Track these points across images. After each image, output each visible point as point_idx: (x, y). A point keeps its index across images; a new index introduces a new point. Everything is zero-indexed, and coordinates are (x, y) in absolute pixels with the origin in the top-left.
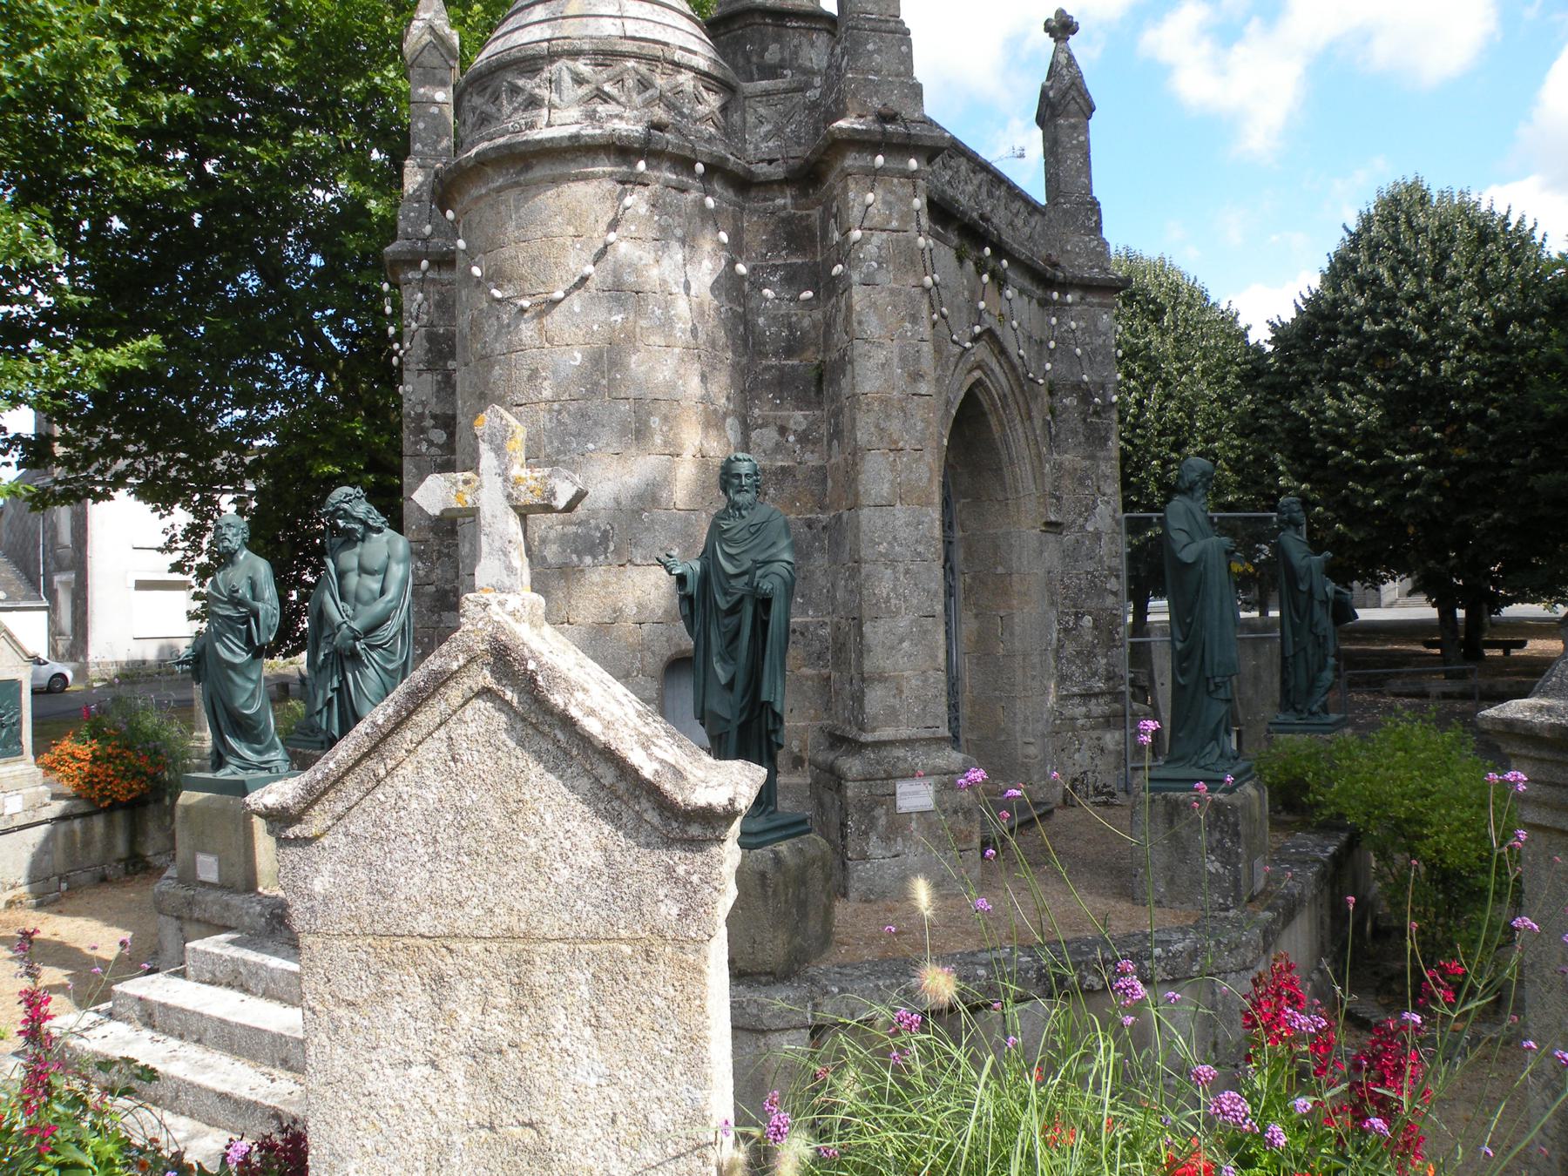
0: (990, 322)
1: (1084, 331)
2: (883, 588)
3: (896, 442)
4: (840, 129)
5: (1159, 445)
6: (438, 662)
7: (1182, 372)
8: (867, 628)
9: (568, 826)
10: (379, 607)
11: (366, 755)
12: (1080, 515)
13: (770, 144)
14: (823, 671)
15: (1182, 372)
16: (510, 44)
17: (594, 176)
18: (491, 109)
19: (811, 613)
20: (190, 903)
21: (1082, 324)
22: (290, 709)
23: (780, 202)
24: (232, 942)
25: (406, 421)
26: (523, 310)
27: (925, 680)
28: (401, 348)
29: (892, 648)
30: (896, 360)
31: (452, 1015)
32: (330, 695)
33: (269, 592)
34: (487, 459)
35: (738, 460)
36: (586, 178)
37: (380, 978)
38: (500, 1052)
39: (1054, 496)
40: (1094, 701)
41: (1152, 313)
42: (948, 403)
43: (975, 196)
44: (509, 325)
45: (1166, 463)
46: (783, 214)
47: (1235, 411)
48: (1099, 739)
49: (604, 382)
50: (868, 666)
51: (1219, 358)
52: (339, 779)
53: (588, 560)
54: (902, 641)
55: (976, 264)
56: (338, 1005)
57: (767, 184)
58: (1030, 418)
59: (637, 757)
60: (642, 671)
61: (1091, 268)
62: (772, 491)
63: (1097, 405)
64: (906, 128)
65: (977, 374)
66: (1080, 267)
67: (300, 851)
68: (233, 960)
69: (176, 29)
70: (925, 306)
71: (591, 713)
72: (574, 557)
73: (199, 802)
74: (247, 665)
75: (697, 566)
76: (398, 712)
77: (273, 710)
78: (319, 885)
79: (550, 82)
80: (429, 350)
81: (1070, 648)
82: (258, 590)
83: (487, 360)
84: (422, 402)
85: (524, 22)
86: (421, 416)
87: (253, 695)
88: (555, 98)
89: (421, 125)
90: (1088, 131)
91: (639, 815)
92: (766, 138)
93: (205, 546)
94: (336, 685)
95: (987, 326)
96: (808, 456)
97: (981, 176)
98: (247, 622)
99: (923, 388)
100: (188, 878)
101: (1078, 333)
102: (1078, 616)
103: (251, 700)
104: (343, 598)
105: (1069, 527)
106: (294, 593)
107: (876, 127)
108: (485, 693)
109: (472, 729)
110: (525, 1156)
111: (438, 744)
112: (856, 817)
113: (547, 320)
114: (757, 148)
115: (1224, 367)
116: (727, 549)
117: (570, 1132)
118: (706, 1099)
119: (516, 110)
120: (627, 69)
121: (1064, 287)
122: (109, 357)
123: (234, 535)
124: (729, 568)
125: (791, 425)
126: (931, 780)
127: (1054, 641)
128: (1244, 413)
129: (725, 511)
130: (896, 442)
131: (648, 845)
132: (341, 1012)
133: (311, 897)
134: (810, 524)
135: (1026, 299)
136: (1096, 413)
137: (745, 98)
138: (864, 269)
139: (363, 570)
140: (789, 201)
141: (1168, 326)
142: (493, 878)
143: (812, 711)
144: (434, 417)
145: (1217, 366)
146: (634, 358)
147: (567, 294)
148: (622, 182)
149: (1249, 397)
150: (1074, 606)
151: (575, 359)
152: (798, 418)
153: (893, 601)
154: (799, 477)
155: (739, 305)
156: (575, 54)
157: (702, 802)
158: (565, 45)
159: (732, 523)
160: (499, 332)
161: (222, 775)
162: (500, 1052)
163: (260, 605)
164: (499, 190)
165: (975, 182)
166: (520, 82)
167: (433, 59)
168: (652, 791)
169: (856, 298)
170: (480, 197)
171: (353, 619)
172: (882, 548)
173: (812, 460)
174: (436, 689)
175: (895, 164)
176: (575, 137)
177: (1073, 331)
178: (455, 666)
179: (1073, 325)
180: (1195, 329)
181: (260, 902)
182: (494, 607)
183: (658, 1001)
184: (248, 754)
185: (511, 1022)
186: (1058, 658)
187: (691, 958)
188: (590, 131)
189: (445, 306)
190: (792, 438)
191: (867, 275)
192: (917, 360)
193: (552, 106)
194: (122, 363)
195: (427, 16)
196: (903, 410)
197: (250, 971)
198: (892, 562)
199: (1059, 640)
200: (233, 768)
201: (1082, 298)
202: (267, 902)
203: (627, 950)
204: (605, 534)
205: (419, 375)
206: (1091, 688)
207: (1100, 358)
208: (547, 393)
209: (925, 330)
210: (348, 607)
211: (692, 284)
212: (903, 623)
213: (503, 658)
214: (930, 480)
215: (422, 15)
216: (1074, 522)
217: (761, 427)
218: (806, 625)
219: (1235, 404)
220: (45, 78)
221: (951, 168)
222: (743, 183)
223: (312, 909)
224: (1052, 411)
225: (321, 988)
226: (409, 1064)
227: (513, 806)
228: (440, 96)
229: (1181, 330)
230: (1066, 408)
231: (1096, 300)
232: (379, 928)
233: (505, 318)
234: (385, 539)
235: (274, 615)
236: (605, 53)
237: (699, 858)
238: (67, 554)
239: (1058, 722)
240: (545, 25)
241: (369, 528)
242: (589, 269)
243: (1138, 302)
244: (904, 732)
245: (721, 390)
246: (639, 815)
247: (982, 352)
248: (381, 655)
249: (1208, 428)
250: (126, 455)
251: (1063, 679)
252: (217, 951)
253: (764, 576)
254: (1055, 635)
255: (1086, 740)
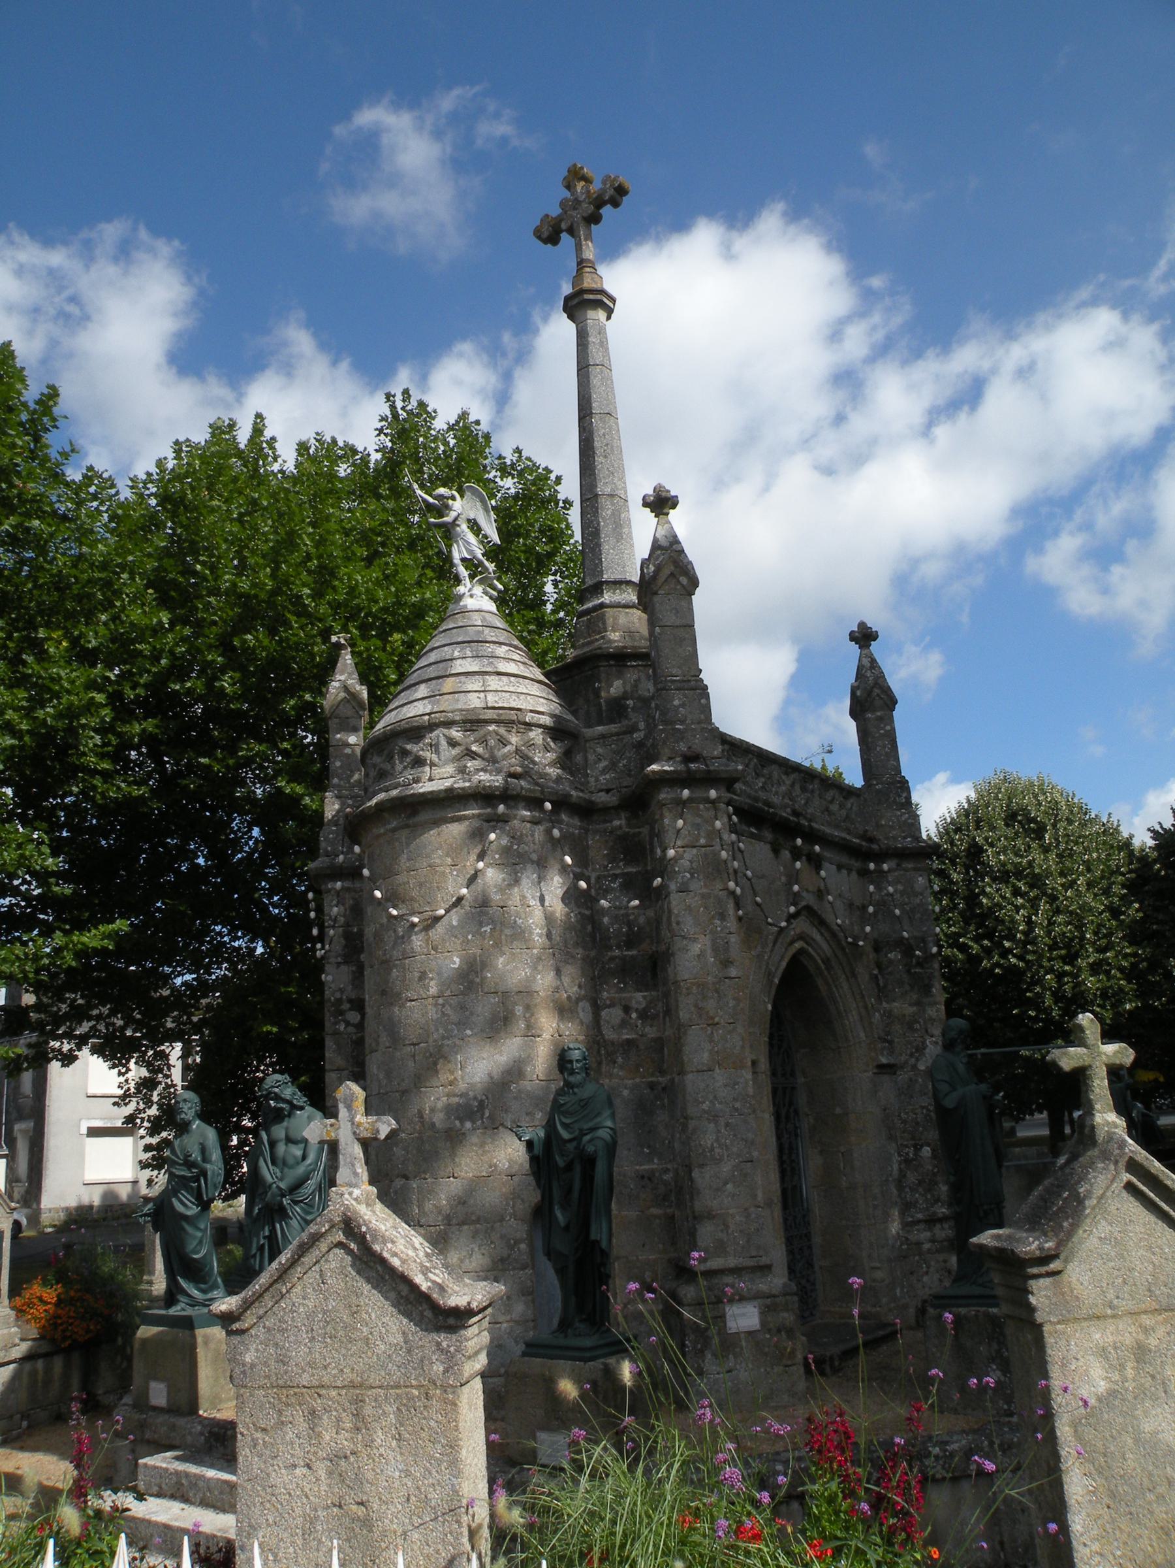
0: (809, 899)
1: (902, 893)
2: (708, 1139)
3: (712, 1018)
4: (653, 772)
5: (1050, 959)
6: (316, 1227)
7: (1065, 886)
8: (695, 1174)
9: (384, 1320)
10: (301, 1169)
11: (275, 1281)
12: (912, 1055)
13: (607, 776)
14: (668, 1211)
15: (1065, 886)
16: (401, 717)
17: (465, 818)
18: (388, 767)
19: (656, 1161)
20: (142, 1426)
21: (900, 887)
22: (230, 1252)
23: (616, 823)
24: (177, 1458)
25: (327, 1005)
26: (413, 925)
27: (748, 1216)
28: (323, 948)
29: (718, 1190)
30: (709, 951)
31: (319, 1435)
32: (262, 1242)
33: (216, 1155)
34: (343, 1112)
35: (570, 1049)
36: (459, 819)
37: (280, 1412)
38: (346, 1457)
39: (886, 1041)
40: (938, 1226)
41: (1034, 831)
42: (769, 975)
43: (789, 794)
44: (403, 937)
45: (1060, 976)
46: (619, 833)
47: (1124, 920)
48: (945, 1261)
49: (478, 980)
50: (698, 1206)
51: (1103, 871)
52: (261, 1295)
53: (468, 1125)
54: (726, 1184)
55: (791, 852)
56: (256, 1431)
57: (606, 811)
58: (854, 975)
59: (419, 1279)
60: (514, 1215)
61: (905, 838)
62: (620, 1060)
63: (918, 957)
64: (706, 765)
65: (798, 945)
66: (895, 838)
67: (239, 1338)
68: (177, 1473)
69: (148, 672)
70: (731, 906)
71: (395, 1255)
72: (457, 1123)
73: (154, 1335)
74: (197, 1217)
75: (542, 1134)
76: (292, 1256)
77: (217, 1254)
78: (248, 1358)
79: (431, 745)
80: (346, 946)
81: (912, 1178)
82: (207, 1153)
83: (387, 964)
84: (340, 989)
85: (411, 699)
86: (339, 1001)
87: (201, 1242)
88: (435, 757)
89: (338, 764)
90: (893, 721)
91: (421, 1313)
92: (604, 772)
93: (155, 1098)
94: (267, 1233)
95: (804, 903)
96: (648, 1029)
97: (794, 776)
98: (198, 1181)
99: (733, 972)
100: (142, 1404)
101: (897, 896)
102: (917, 1148)
103: (200, 1246)
104: (274, 1163)
105: (902, 1067)
106: (235, 1138)
107: (681, 767)
108: (340, 1245)
109: (333, 1265)
110: (359, 1524)
111: (314, 1275)
112: (692, 1337)
113: (432, 933)
114: (597, 780)
115: (1109, 878)
116: (564, 1120)
117: (384, 1507)
118: (459, 1484)
119: (405, 768)
120: (490, 732)
121: (880, 857)
122: (85, 939)
123: (190, 1108)
124: (565, 1135)
125: (634, 1004)
126: (756, 1303)
127: (896, 1172)
128: (1134, 921)
129: (562, 1089)
130: (712, 1018)
131: (426, 1330)
132: (258, 1435)
133: (244, 1365)
134: (652, 1086)
135: (845, 872)
136: (920, 964)
137: (586, 741)
138: (680, 880)
139: (289, 1140)
140: (623, 822)
141: (1050, 843)
142: (344, 1351)
143: (661, 1246)
144: (350, 1001)
145: (1102, 877)
146: (501, 960)
147: (447, 911)
148: (488, 821)
149: (1137, 905)
150: (913, 1138)
151: (455, 963)
152: (639, 999)
153: (717, 1150)
154: (642, 1047)
155: (587, 908)
156: (449, 724)
157: (453, 1305)
158: (441, 717)
159: (567, 1098)
160: (395, 943)
161: (174, 1311)
162: (346, 1457)
163: (208, 1166)
164: (394, 830)
165: (788, 782)
166: (409, 747)
167: (348, 711)
168: (425, 1298)
169: (674, 903)
170: (379, 836)
171: (281, 1179)
172: (705, 1106)
173: (651, 1032)
174: (313, 1243)
175: (699, 794)
176: (449, 790)
177: (892, 895)
178: (323, 1230)
179: (891, 889)
180: (1076, 843)
181: (200, 1423)
182: (346, 1196)
183: (432, 1423)
184: (195, 1293)
185: (352, 1438)
186: (900, 1186)
187: (451, 1396)
188: (461, 784)
189: (357, 912)
190: (634, 1015)
191: (683, 883)
192: (727, 950)
193: (432, 765)
194: (95, 944)
195: (342, 678)
196: (717, 991)
197: (191, 1482)
198: (714, 1117)
199: (901, 1170)
200: (183, 1305)
201: (898, 865)
202: (206, 1422)
203: (416, 1392)
204: (481, 1103)
205: (338, 967)
206: (935, 1213)
207: (918, 916)
208: (433, 990)
209: (732, 924)
210: (277, 1170)
211: (546, 897)
212: (726, 1168)
213: (350, 1226)
214: (743, 1047)
215: (338, 677)
216: (906, 1062)
217: (609, 1007)
218: (653, 1171)
219: (1124, 913)
220: (52, 727)
221: (763, 776)
222: (586, 811)
223: (244, 1372)
224: (879, 966)
225: (247, 1420)
226: (295, 1466)
227: (355, 1309)
228: (352, 739)
229: (1062, 846)
230: (891, 962)
231: (910, 866)
232: (281, 1382)
233: (400, 931)
234: (306, 1115)
235: (219, 1174)
236: (471, 722)
237: (454, 1337)
238: (27, 1103)
239: (905, 1247)
240: (426, 701)
241: (294, 1107)
242: (464, 891)
243: (1020, 822)
244: (732, 1262)
245: (571, 984)
246: (421, 1313)
247: (802, 925)
248: (302, 1208)
249: (1099, 939)
250: (90, 1019)
251: (906, 1207)
252: (164, 1465)
253: (590, 1141)
254: (896, 1167)
255: (933, 1263)
